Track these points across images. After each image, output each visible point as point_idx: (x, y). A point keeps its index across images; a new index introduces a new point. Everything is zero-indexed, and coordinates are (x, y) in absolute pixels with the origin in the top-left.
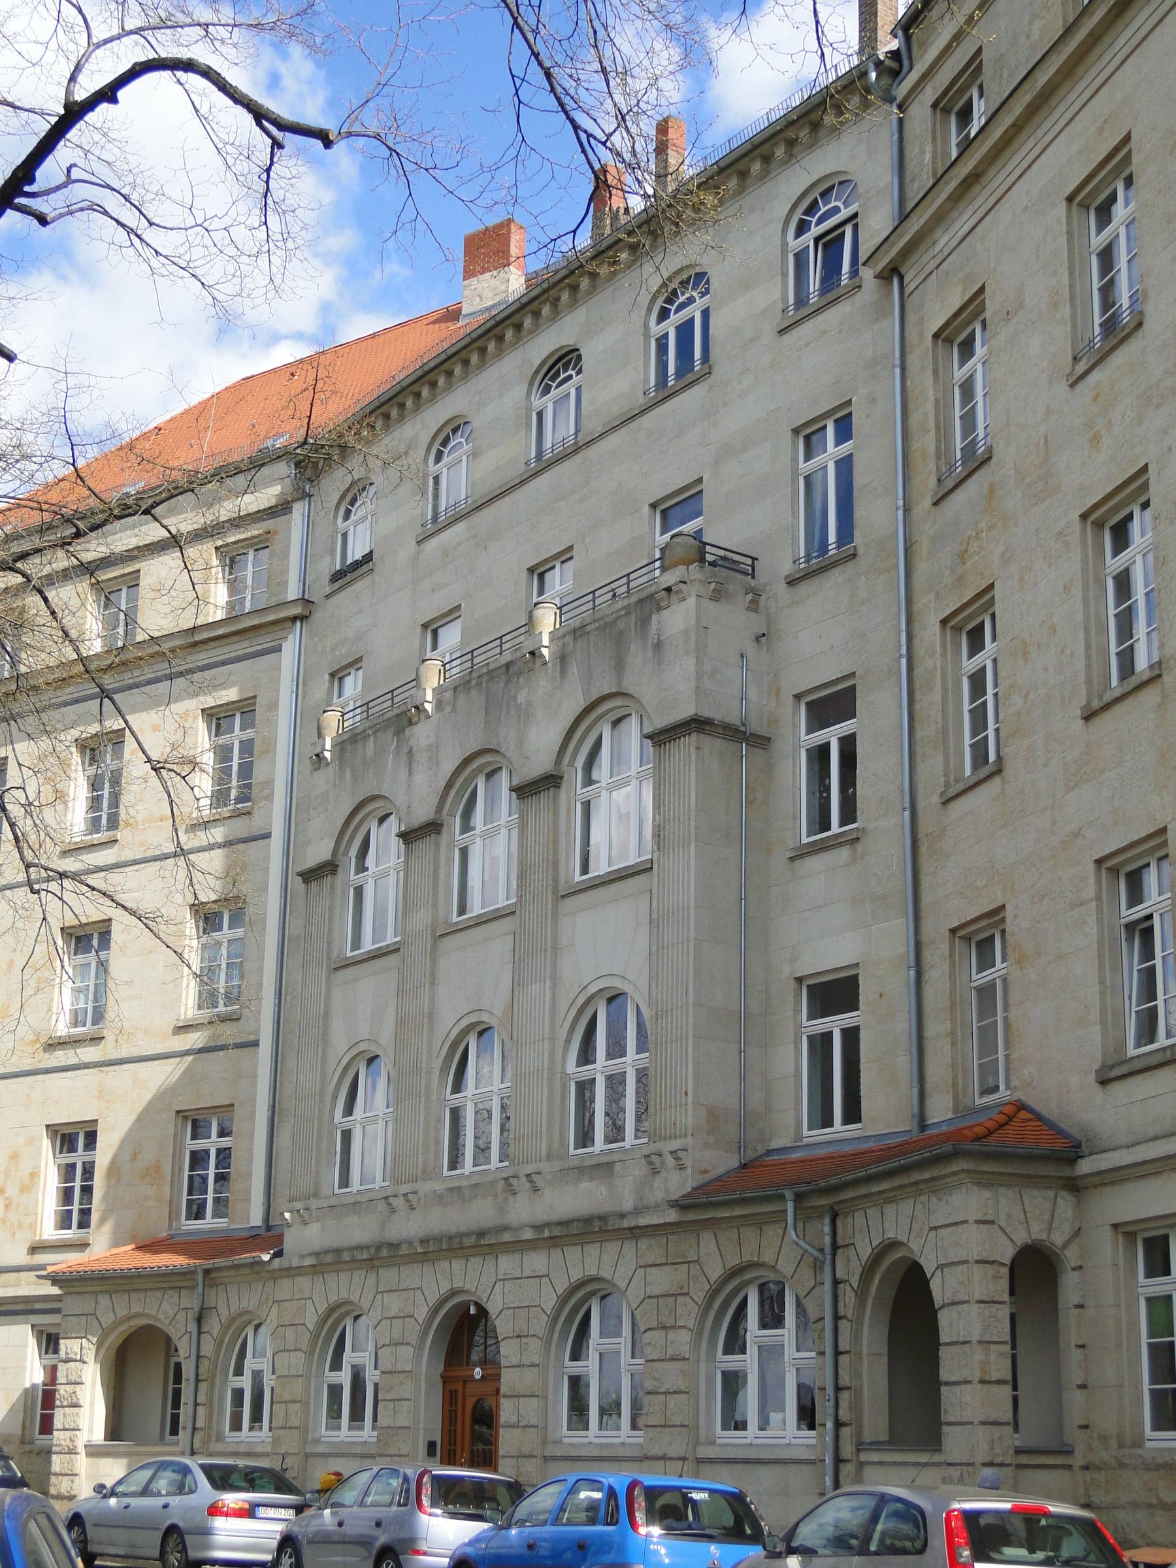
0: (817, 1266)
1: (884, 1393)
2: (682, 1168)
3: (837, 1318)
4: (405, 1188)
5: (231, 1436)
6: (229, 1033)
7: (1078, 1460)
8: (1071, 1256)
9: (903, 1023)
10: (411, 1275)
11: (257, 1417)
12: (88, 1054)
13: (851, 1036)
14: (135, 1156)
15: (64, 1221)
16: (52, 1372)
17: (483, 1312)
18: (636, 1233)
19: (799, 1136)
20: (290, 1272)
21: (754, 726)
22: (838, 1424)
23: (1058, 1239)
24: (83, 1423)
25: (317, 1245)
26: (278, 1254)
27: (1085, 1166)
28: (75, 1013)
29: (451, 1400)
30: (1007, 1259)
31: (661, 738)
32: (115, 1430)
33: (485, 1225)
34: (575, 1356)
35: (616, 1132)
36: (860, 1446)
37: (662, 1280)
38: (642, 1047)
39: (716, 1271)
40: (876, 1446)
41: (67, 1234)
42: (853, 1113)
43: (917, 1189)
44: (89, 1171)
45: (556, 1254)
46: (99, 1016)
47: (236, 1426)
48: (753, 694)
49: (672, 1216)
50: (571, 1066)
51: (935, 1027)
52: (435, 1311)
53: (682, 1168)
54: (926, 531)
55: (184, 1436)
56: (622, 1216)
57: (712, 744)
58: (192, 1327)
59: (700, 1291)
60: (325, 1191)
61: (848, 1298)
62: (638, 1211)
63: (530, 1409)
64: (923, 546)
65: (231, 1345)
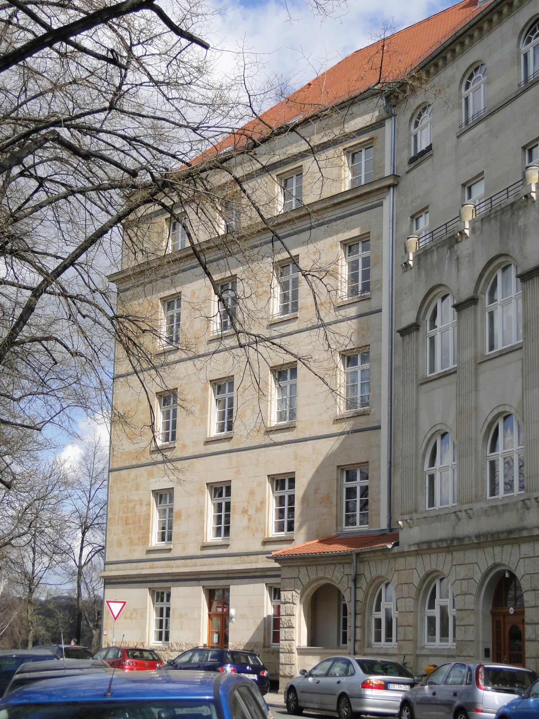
4: (466, 507)
6: (363, 422)
10: (471, 556)
15: (280, 528)
17: (513, 576)
20: (403, 554)
24: (296, 637)
25: (417, 540)
26: (397, 544)
32: (313, 640)
33: (512, 526)
41: (282, 534)
46: (293, 414)
52: (485, 575)
55: (350, 644)
58: (351, 585)
60: (421, 509)
65: (373, 595)
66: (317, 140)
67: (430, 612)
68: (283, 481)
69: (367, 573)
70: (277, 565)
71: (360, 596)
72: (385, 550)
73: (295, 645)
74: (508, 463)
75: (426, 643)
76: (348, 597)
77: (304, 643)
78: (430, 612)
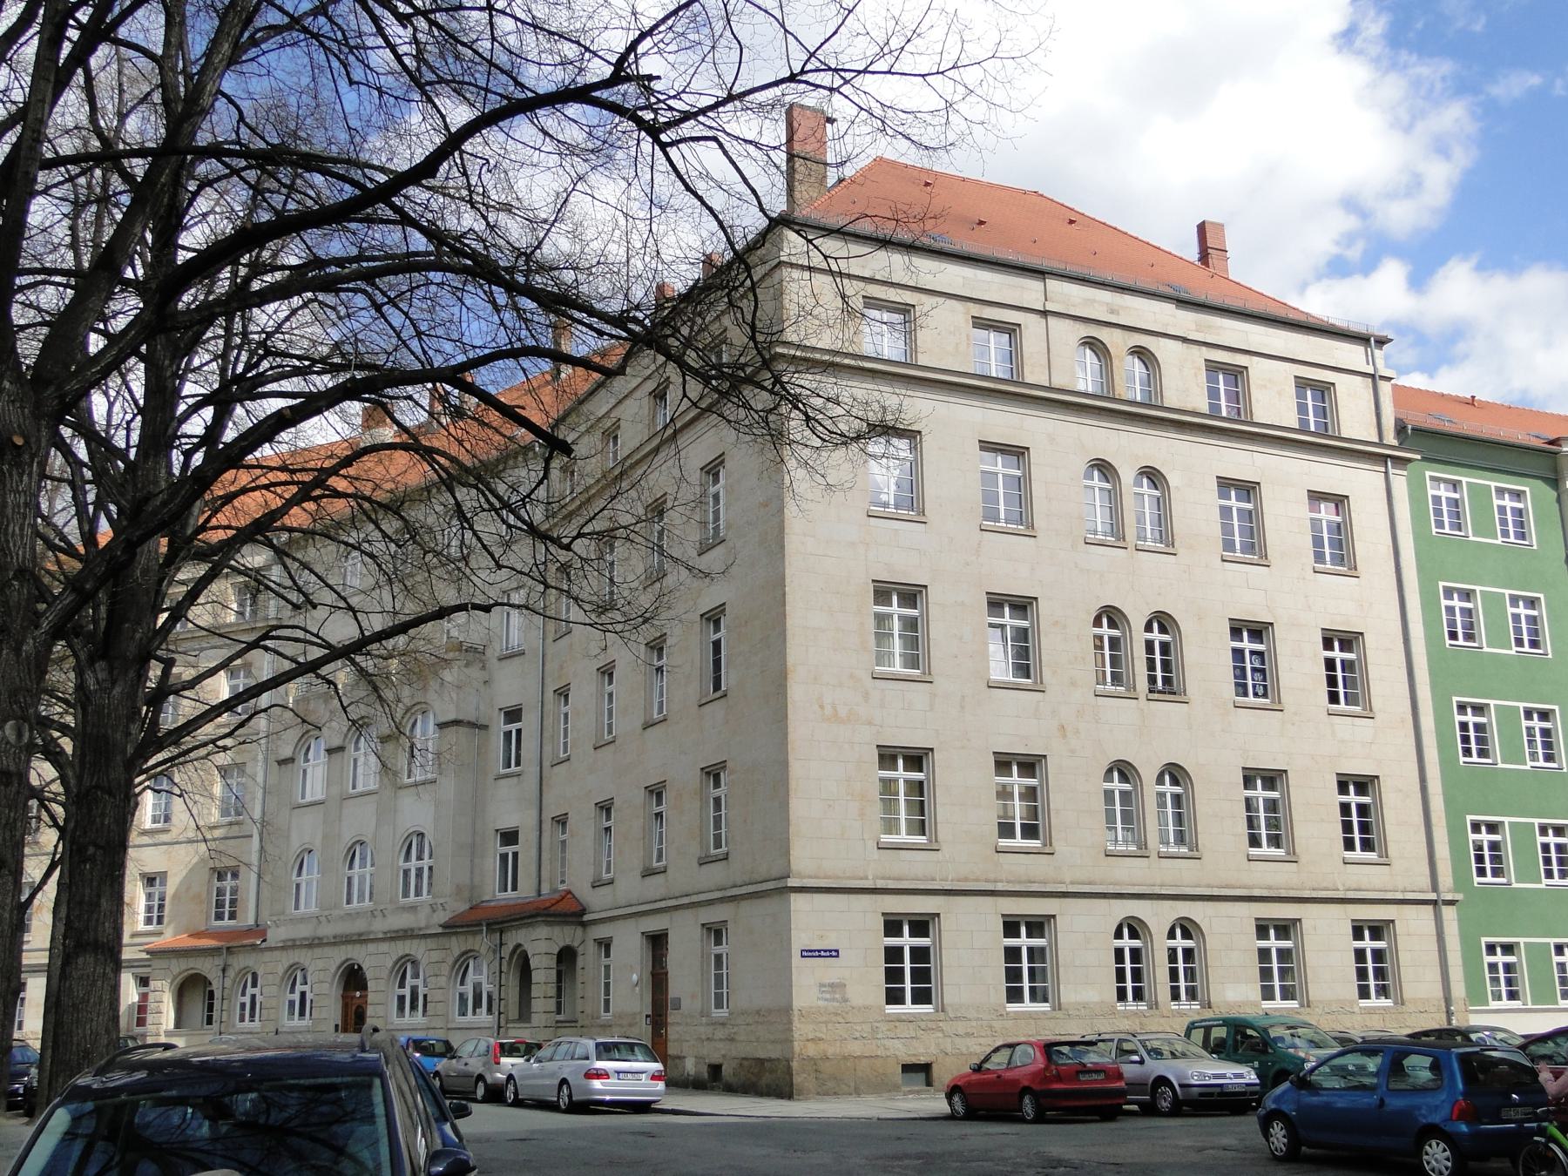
0: (494, 952)
1: (517, 999)
2: (444, 910)
3: (501, 972)
4: (326, 913)
5: (239, 1025)
6: (235, 830)
7: (579, 1025)
8: (580, 950)
9: (534, 852)
10: (328, 951)
11: (252, 1015)
12: (164, 838)
13: (515, 855)
14: (188, 889)
15: (149, 921)
16: (144, 997)
17: (360, 968)
18: (425, 936)
19: (494, 895)
20: (271, 949)
21: (482, 721)
22: (500, 1013)
23: (576, 944)
24: (163, 1021)
25: (283, 938)
26: (264, 941)
27: (586, 918)
28: (154, 816)
29: (346, 1007)
30: (556, 952)
31: (442, 726)
32: (178, 1024)
33: (362, 930)
34: (400, 987)
35: (417, 893)
36: (507, 1022)
37: (435, 956)
38: (431, 857)
39: (457, 953)
40: (513, 1021)
41: (150, 928)
42: (515, 888)
43: (530, 925)
44: (162, 899)
45: (393, 943)
46: (167, 819)
47: (242, 1019)
48: (482, 708)
49: (440, 930)
50: (401, 863)
51: (545, 856)
52: (339, 967)
53: (444, 910)
54: (549, 652)
55: (215, 1025)
56: (420, 929)
57: (462, 730)
58: (220, 974)
59: (450, 960)
60: (288, 912)
61: (505, 963)
62: (427, 927)
63: (380, 1010)
64: (548, 657)
65: (240, 982)
66: (205, 645)
67: (292, 997)
68: (154, 879)
69: (235, 965)
70: (144, 956)
71: (228, 983)
72: (253, 946)
73: (164, 1027)
74: (362, 882)
75: (713, 1010)
76: (216, 986)
77: (171, 1025)
78: (292, 997)
